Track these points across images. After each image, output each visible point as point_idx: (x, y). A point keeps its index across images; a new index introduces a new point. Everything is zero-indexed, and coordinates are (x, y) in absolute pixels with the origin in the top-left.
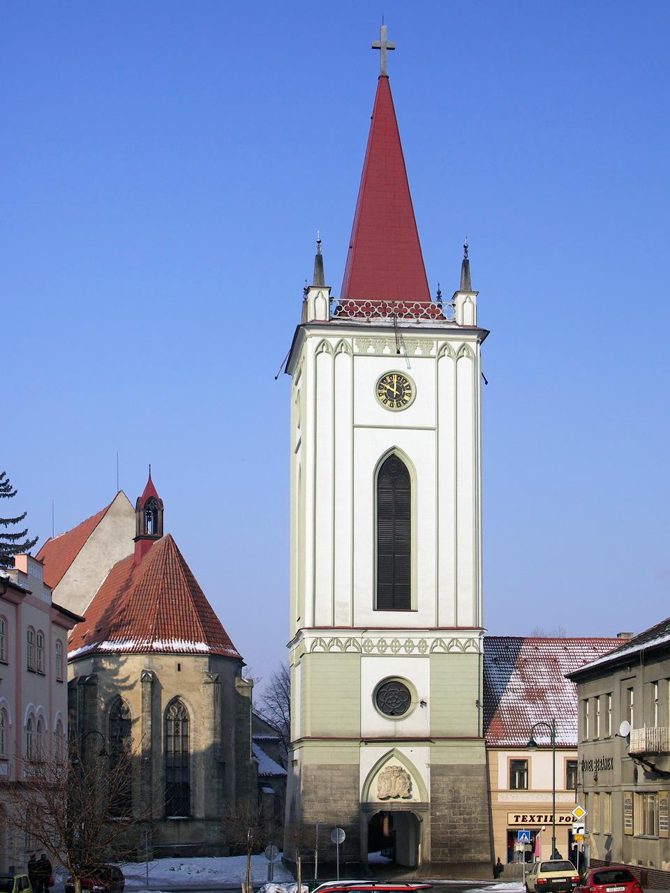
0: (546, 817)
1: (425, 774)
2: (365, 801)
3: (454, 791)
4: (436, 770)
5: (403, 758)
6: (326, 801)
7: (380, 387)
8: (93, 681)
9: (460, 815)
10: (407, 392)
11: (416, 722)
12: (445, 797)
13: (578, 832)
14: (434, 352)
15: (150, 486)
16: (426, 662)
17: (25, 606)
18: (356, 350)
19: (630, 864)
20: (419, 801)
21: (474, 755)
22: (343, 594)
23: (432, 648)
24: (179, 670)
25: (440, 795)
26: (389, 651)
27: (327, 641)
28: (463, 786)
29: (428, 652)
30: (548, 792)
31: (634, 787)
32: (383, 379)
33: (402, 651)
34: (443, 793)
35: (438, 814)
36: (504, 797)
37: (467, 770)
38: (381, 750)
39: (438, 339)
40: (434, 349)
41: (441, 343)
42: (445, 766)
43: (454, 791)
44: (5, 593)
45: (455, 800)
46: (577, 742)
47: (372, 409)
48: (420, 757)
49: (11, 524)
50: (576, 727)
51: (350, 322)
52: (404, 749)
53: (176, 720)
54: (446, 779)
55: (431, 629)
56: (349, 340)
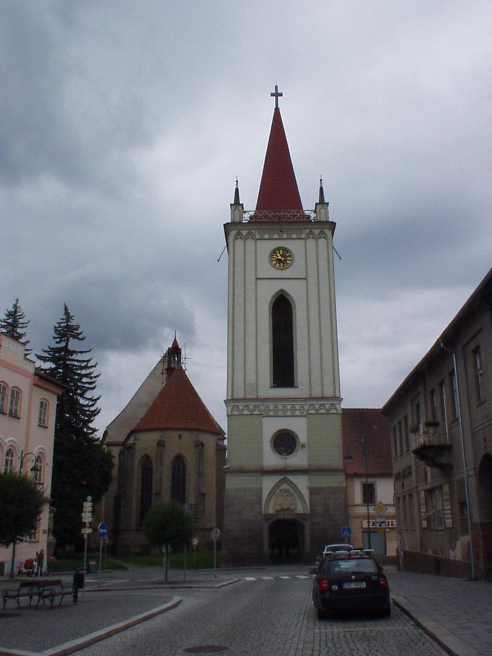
0: (389, 522)
1: (306, 493)
4: (313, 491)
5: (291, 483)
7: (271, 256)
10: (288, 258)
11: (299, 459)
13: (380, 526)
15: (175, 341)
18: (258, 236)
19: (428, 554)
20: (302, 512)
22: (251, 378)
27: (241, 407)
31: (425, 486)
35: (315, 521)
37: (333, 491)
38: (276, 479)
41: (308, 231)
47: (266, 269)
48: (302, 483)
49: (79, 354)
50: (431, 481)
52: (293, 478)
55: (306, 399)
56: (253, 231)
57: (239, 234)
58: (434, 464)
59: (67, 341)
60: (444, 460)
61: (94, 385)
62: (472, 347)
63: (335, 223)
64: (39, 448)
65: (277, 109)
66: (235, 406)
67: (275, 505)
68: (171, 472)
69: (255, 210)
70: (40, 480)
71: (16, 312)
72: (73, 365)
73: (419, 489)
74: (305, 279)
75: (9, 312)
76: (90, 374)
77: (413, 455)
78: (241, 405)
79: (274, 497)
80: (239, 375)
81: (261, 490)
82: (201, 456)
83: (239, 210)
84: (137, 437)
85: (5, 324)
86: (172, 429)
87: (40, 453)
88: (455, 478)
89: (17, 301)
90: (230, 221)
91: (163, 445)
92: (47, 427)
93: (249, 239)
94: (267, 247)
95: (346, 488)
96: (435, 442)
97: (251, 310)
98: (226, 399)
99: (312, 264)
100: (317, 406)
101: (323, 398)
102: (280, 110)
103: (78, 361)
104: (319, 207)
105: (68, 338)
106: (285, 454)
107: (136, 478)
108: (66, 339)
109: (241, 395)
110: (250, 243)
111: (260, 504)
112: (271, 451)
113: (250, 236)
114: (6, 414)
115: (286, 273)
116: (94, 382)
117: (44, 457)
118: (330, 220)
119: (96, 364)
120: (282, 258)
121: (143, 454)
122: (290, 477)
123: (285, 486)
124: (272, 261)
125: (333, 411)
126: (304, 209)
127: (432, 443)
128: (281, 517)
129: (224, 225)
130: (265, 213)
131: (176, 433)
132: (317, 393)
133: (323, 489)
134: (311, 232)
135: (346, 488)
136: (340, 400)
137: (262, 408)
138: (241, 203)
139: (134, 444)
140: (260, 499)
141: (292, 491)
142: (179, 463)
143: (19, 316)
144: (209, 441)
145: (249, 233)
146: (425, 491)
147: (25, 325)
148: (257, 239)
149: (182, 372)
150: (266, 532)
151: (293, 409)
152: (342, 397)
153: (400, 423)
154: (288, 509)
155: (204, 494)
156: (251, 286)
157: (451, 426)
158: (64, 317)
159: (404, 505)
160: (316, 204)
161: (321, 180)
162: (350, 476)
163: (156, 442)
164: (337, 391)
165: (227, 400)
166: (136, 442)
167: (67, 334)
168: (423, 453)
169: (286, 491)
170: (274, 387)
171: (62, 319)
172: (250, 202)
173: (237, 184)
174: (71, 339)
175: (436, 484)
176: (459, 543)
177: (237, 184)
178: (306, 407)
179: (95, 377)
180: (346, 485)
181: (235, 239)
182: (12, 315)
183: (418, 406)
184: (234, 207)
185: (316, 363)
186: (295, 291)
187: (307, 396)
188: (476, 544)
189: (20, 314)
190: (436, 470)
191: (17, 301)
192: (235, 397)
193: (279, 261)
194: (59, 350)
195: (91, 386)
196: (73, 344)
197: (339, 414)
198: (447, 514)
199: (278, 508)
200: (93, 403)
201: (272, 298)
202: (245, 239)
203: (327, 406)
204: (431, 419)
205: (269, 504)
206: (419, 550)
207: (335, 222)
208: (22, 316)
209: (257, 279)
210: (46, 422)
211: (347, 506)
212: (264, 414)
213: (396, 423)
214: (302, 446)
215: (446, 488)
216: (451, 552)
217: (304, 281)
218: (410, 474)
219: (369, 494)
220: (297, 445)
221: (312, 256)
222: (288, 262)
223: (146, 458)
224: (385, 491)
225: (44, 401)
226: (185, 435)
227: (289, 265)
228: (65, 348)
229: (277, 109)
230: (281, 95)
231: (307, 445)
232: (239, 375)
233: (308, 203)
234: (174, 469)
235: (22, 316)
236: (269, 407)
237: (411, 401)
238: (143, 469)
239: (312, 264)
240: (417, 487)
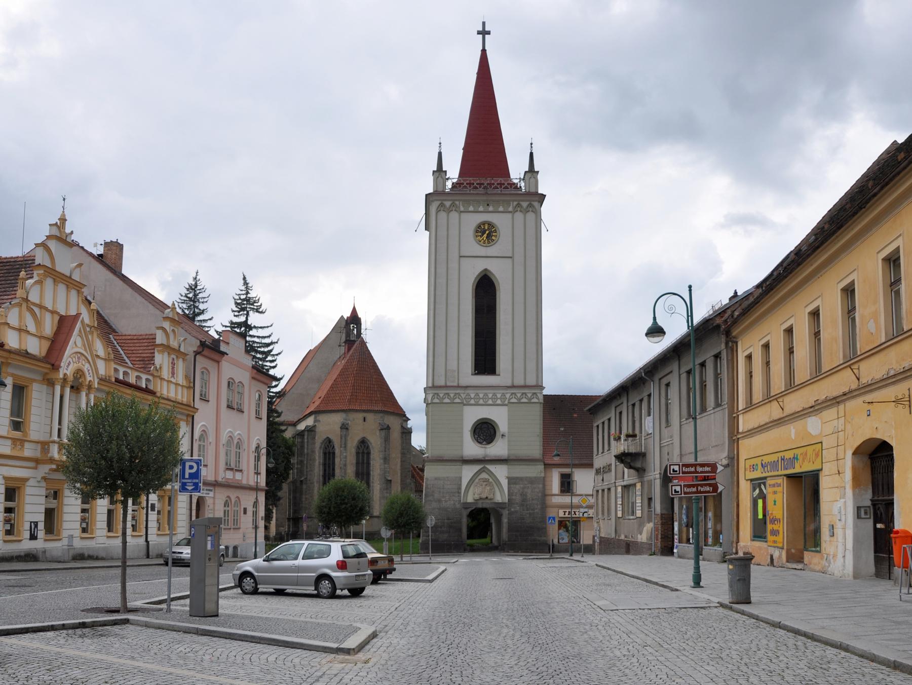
1: (504, 483)
2: (465, 501)
3: (523, 495)
4: (512, 481)
5: (491, 473)
6: (439, 501)
8: (313, 429)
9: (527, 510)
10: (494, 234)
11: (498, 448)
12: (518, 498)
14: (511, 209)
16: (506, 408)
17: (224, 364)
18: (462, 209)
20: (501, 501)
21: (536, 471)
22: (453, 365)
23: (509, 399)
24: (364, 421)
25: (514, 497)
26: (481, 402)
28: (529, 491)
29: (506, 402)
32: (479, 226)
33: (490, 402)
34: (516, 496)
35: (512, 510)
36: (559, 500)
37: (532, 481)
38: (476, 468)
39: (514, 201)
40: (511, 206)
41: (515, 203)
42: (517, 478)
43: (523, 495)
44: (203, 351)
45: (524, 500)
46: (103, 251)
47: (472, 246)
48: (501, 472)
49: (260, 330)
51: (852, 395)
52: (491, 468)
53: (363, 453)
54: (518, 486)
55: (508, 387)
56: (457, 203)
57: (442, 205)
58: (630, 467)
59: (248, 315)
60: (638, 465)
61: (275, 363)
62: (664, 381)
63: (545, 196)
64: (227, 433)
65: (484, 51)
66: (436, 393)
67: (474, 494)
68: (355, 457)
69: (457, 177)
70: (239, 467)
71: (196, 286)
72: (254, 342)
73: (617, 484)
74: (511, 257)
75: (189, 286)
76: (271, 351)
77: (614, 458)
78: (441, 393)
79: (472, 487)
80: (440, 361)
83: (441, 177)
84: (318, 418)
85: (185, 299)
86: (356, 411)
87: (230, 436)
88: (645, 479)
89: (197, 273)
90: (431, 191)
91: (347, 429)
92: (208, 401)
93: (452, 212)
94: (473, 220)
95: (544, 478)
96: (633, 450)
98: (425, 386)
100: (519, 395)
101: (525, 387)
102: (487, 52)
103: (258, 337)
104: (529, 175)
105: (248, 312)
106: (484, 443)
107: (317, 463)
108: (245, 312)
109: (442, 383)
110: (454, 215)
111: (459, 493)
112: (471, 440)
114: (234, 409)
115: (492, 250)
116: (275, 361)
117: (206, 435)
118: (539, 192)
119: (278, 340)
121: (325, 437)
122: (488, 467)
123: (484, 475)
124: (477, 236)
125: (535, 400)
126: (512, 177)
127: (630, 451)
128: (480, 506)
129: (426, 195)
130: (470, 180)
131: (361, 416)
132: (519, 381)
134: (519, 205)
135: (544, 478)
136: (542, 388)
137: (463, 396)
138: (444, 169)
139: (314, 426)
140: (460, 488)
141: (491, 480)
142: (363, 449)
143: (200, 290)
144: (394, 422)
145: (453, 205)
146: (622, 486)
147: (205, 300)
148: (461, 212)
149: (363, 344)
150: (465, 520)
151: (494, 397)
152: (544, 386)
154: (487, 498)
155: (391, 481)
156: (454, 265)
157: (647, 437)
158: (243, 288)
159: (603, 496)
160: (526, 172)
161: (531, 144)
163: (340, 425)
164: (540, 380)
165: (427, 387)
166: (316, 424)
167: (246, 308)
168: (625, 458)
169: (486, 480)
170: (475, 374)
171: (242, 290)
172: (453, 170)
173: (440, 147)
174: (251, 313)
175: (632, 482)
176: (645, 529)
177: (440, 147)
178: (508, 396)
179: (277, 355)
180: (545, 474)
181: (438, 211)
182: (192, 289)
183: (621, 413)
184: (437, 174)
186: (500, 272)
187: (509, 384)
188: (656, 529)
189: (201, 287)
190: (632, 471)
191: (197, 273)
192: (436, 384)
193: (489, 236)
194: (239, 325)
195: (273, 364)
196: (254, 319)
197: (541, 403)
198: (638, 506)
199: (477, 497)
200: (277, 383)
201: (476, 278)
202: (449, 211)
203: (529, 395)
204: (631, 432)
205: (325, 470)
206: (613, 536)
207: (544, 194)
208: (203, 290)
209: (461, 257)
210: (207, 397)
211: (545, 495)
212: (465, 402)
213: (599, 422)
214: (502, 435)
215: (639, 486)
216: (639, 536)
217: (510, 259)
218: (610, 470)
219: (567, 485)
220: (497, 434)
222: (493, 238)
223: (329, 441)
224: (584, 481)
225: (231, 380)
226: (370, 417)
227: (495, 242)
228: (245, 324)
229: (484, 51)
230: (489, 33)
231: (507, 435)
232: (440, 361)
233: (517, 169)
234: (358, 453)
235: (203, 290)
236: (470, 395)
237: (616, 407)
238: (325, 454)
240: (615, 483)
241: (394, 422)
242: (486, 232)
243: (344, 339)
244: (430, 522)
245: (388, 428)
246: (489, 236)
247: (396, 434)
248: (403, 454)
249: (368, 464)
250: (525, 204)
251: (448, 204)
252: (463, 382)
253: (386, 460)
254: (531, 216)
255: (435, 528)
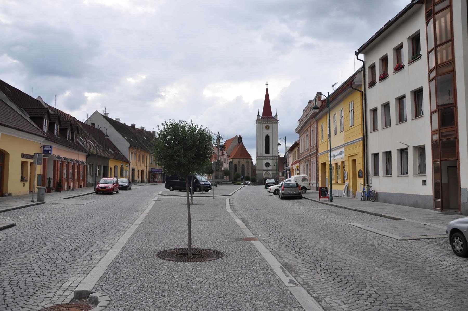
1: (271, 174)
4: (272, 174)
5: (269, 172)
11: (270, 168)
22: (261, 152)
30: (186, 204)
47: (265, 130)
48: (270, 172)
52: (269, 171)
57: (259, 122)
65: (267, 89)
81: (263, 173)
82: (248, 164)
94: (265, 125)
97: (261, 138)
99: (274, 129)
110: (261, 124)
113: (261, 122)
115: (269, 131)
120: (267, 127)
123: (267, 173)
131: (242, 159)
133: (274, 173)
140: (263, 175)
144: (249, 160)
151: (269, 158)
153: (398, 49)
162: (279, 171)
172: (261, 115)
185: (274, 149)
186: (270, 135)
193: (268, 128)
202: (260, 123)
221: (274, 127)
223: (236, 165)
226: (244, 159)
229: (267, 89)
233: (273, 115)
234: (242, 167)
238: (235, 167)
239: (274, 129)
241: (249, 160)
242: (267, 127)
243: (238, 142)
244: (257, 181)
245: (248, 162)
246: (268, 128)
247: (250, 163)
248: (251, 167)
249: (244, 170)
250: (275, 122)
251: (260, 122)
252: (263, 155)
253: (248, 169)
254: (276, 124)
255: (258, 182)
